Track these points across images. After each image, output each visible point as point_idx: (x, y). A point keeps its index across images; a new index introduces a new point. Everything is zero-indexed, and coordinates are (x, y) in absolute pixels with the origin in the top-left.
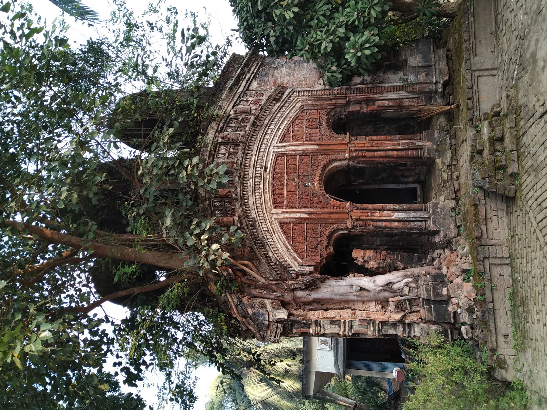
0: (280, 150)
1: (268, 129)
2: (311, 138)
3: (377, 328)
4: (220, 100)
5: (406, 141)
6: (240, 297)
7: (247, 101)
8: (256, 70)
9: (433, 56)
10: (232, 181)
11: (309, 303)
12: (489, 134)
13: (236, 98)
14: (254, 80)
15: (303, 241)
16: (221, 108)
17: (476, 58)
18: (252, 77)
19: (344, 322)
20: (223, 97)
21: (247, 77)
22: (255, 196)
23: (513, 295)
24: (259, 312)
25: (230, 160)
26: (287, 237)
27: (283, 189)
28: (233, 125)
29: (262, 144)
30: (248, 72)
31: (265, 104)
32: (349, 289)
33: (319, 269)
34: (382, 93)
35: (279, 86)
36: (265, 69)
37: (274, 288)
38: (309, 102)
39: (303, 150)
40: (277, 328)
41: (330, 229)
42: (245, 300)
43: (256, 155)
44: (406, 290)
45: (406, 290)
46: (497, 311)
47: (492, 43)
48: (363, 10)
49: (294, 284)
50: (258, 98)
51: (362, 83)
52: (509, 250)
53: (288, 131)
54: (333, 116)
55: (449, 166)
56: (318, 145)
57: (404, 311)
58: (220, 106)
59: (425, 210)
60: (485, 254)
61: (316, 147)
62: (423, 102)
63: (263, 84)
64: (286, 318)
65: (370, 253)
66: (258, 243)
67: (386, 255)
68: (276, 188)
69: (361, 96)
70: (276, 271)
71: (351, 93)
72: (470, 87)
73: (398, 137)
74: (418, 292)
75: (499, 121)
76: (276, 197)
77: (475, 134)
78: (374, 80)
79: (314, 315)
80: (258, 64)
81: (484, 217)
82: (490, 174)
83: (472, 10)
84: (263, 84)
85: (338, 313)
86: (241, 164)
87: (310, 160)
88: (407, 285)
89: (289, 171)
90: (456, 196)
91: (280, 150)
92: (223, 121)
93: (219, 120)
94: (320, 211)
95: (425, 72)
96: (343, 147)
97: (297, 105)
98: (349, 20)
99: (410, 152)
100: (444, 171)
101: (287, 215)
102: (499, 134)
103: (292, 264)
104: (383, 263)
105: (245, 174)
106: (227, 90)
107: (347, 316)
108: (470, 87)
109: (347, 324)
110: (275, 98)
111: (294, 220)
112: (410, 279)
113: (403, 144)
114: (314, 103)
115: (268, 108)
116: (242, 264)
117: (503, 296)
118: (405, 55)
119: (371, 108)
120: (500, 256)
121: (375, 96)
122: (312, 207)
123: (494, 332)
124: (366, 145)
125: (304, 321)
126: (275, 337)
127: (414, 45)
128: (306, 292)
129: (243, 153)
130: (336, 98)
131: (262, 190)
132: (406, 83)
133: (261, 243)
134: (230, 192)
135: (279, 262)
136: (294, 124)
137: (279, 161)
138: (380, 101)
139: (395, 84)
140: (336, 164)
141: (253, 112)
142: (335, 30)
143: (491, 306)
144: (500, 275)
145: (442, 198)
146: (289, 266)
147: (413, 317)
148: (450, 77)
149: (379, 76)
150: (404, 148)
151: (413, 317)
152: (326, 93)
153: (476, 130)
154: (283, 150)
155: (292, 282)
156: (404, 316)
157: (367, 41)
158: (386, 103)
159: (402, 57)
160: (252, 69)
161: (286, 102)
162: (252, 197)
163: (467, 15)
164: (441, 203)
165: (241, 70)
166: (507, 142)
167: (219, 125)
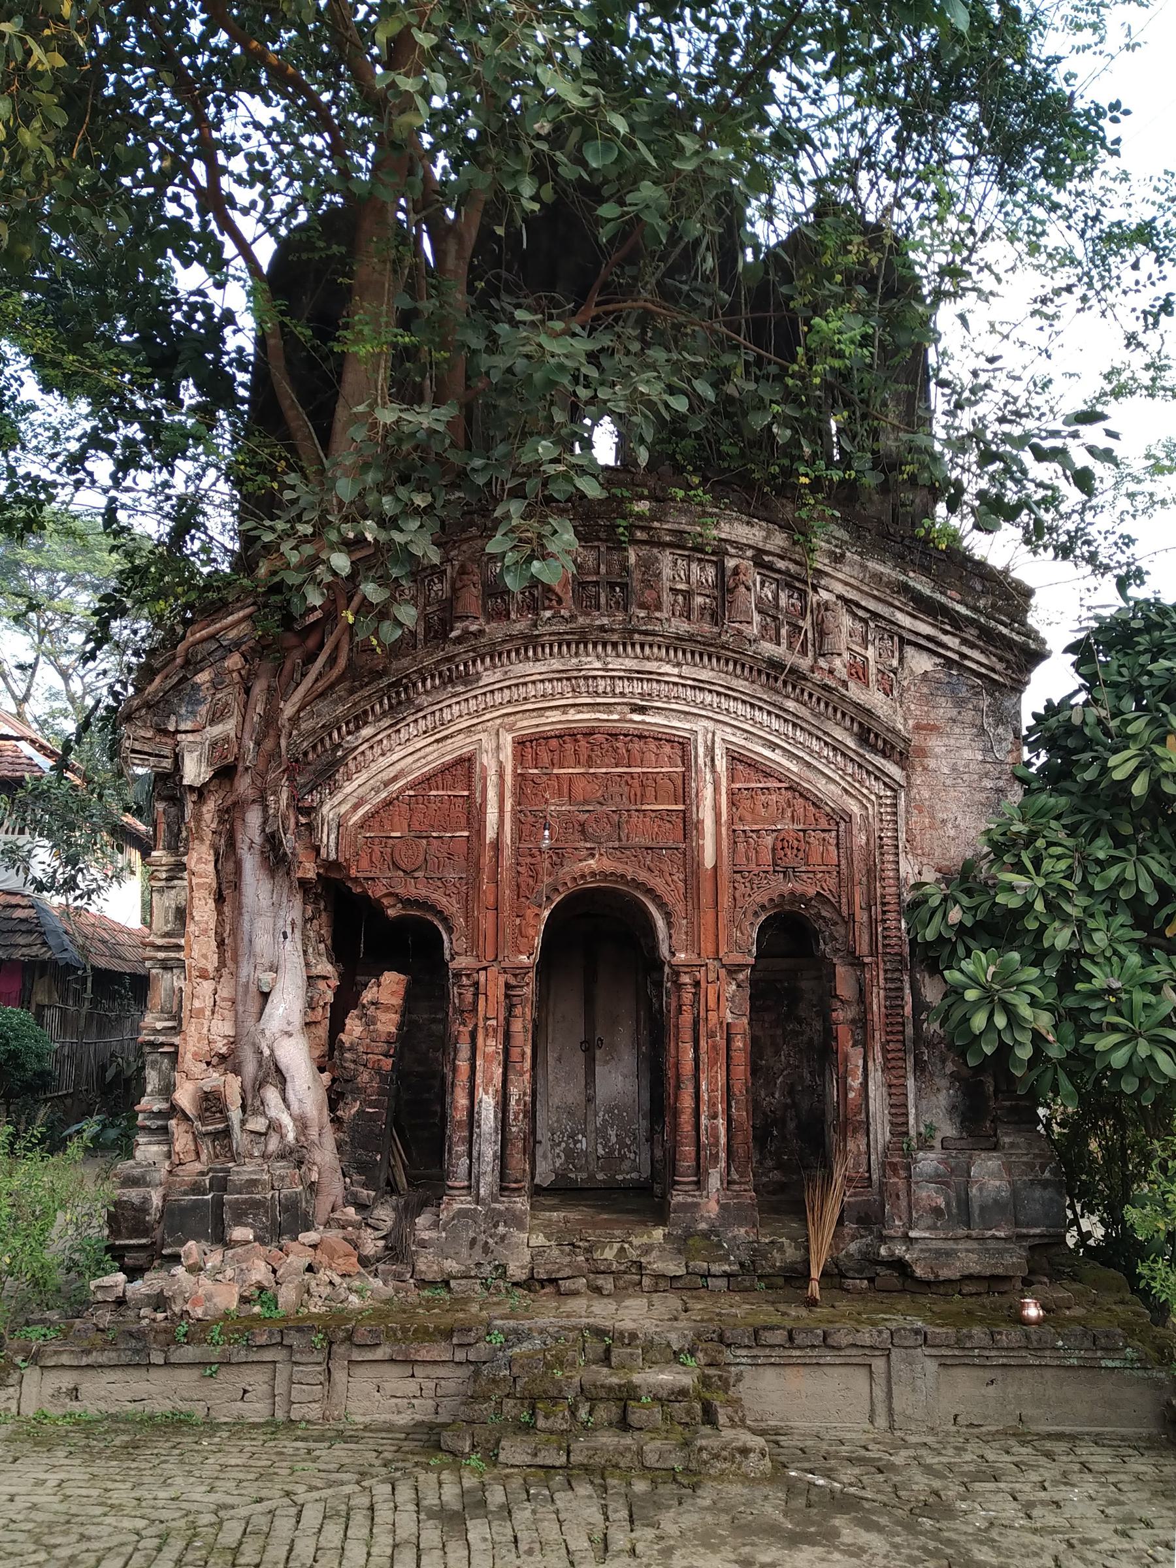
0: (701, 751)
1: (769, 713)
2: (741, 847)
3: (161, 1039)
4: (860, 554)
5: (723, 1140)
6: (244, 648)
7: (865, 643)
8: (974, 666)
9: (1002, 1234)
10: (598, 608)
11: (231, 843)
12: (649, 1385)
13: (872, 605)
14: (938, 661)
15: (416, 825)
16: (838, 559)
17: (931, 1366)
18: (949, 654)
19: (179, 948)
20: (872, 565)
21: (946, 639)
22: (550, 680)
23: (177, 1423)
24: (199, 702)
25: (667, 598)
26: (427, 781)
27: (578, 763)
29: (719, 694)
30: (964, 641)
31: (843, 698)
32: (265, 961)
36: (977, 694)
37: (268, 744)
39: (700, 822)
40: (157, 756)
41: (451, 906)
42: (234, 661)
46: (142, 1373)
47: (986, 1417)
48: (1125, 1009)
49: (277, 802)
50: (872, 678)
51: (920, 1005)
53: (767, 775)
54: (819, 916)
55: (640, 1266)
57: (200, 1118)
58: (843, 555)
59: (502, 1189)
60: (301, 1352)
61: (709, 861)
63: (925, 690)
64: (186, 782)
65: (388, 1023)
66: (398, 694)
67: (378, 1071)
68: (583, 743)
69: (877, 1002)
70: (314, 748)
71: (886, 971)
72: (830, 1341)
73: (740, 1114)
74: (251, 1156)
75: (687, 1420)
76: (554, 743)
77: (669, 1345)
78: (930, 1044)
80: (993, 670)
81: (413, 1357)
82: (520, 1383)
83: (1103, 1363)
84: (925, 690)
85: (206, 930)
86: (646, 633)
87: (670, 844)
88: (274, 1126)
89: (636, 783)
90: (543, 1283)
91: (701, 751)
92: (793, 568)
93: (797, 557)
94: (505, 875)
95: (948, 1204)
96: (708, 946)
97: (851, 801)
98: (1096, 964)
99: (688, 1149)
100: (622, 1249)
101: (492, 779)
102: (637, 1416)
104: (354, 1062)
105: (615, 645)
109: (173, 955)
110: (869, 730)
111: (479, 800)
112: (291, 1136)
113: (715, 1128)
114: (856, 854)
116: (336, 648)
117: (186, 1395)
118: (1012, 1145)
119: (844, 1034)
121: (878, 1048)
122: (517, 852)
125: (184, 834)
126: (134, 751)
127: (1047, 1174)
128: (258, 839)
129: (679, 638)
131: (570, 701)
132: (914, 1143)
133: (400, 703)
134: (560, 601)
135: (344, 757)
136: (789, 794)
137: (667, 749)
138: (861, 1062)
139: (912, 1111)
140: (660, 923)
141: (822, 663)
142: (1066, 919)
143: (157, 1358)
144: (245, 1391)
145: (539, 1240)
146: (335, 788)
147: (182, 1141)
148: (928, 1283)
149: (943, 1062)
151: (182, 1141)
152: (888, 890)
153: (681, 1350)
155: (284, 796)
156: (186, 1118)
157: (1014, 1019)
158: (855, 1083)
159: (1007, 1134)
161: (860, 766)
162: (544, 669)
163: (1087, 1343)
165: (967, 618)
166: (608, 1440)
167: (782, 558)
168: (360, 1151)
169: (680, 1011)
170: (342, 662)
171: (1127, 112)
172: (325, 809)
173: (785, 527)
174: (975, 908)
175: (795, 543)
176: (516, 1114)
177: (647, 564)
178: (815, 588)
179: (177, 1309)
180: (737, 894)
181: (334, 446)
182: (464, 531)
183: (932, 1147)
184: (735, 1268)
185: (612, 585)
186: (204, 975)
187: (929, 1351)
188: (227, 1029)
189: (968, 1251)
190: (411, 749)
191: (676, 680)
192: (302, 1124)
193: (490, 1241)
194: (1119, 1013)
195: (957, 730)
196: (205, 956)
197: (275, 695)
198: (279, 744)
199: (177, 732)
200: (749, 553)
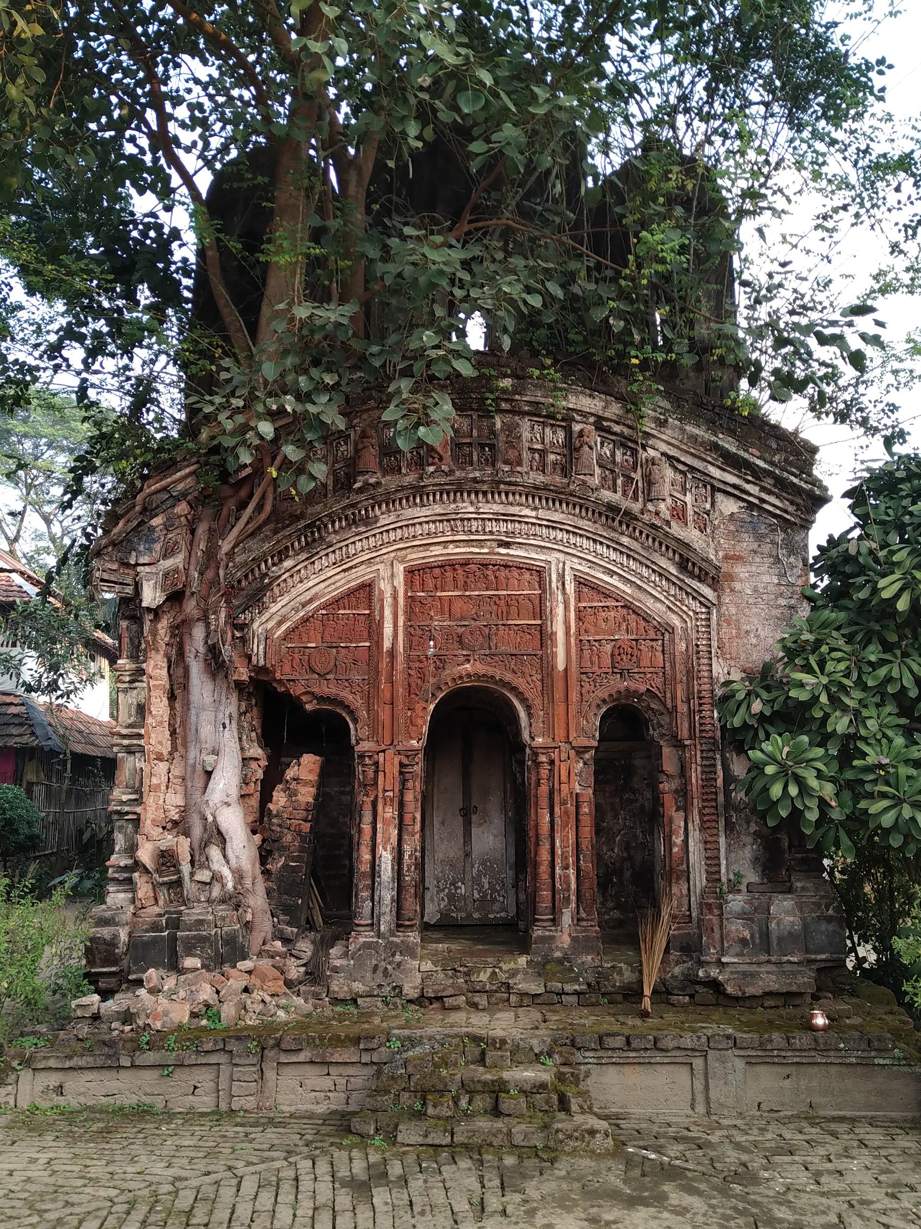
0: (554, 577)
1: (608, 547)
2: (587, 653)
3: (127, 809)
4: (680, 420)
5: (573, 886)
6: (189, 497)
7: (684, 490)
8: (771, 508)
9: (795, 959)
12: (516, 1081)
13: (689, 460)
15: (327, 638)
16: (662, 424)
17: (740, 1064)
18: (751, 499)
19: (140, 736)
20: (689, 428)
21: (748, 487)
23: (141, 1113)
24: (154, 541)
25: (526, 455)
26: (336, 602)
27: (456, 587)
28: (619, 458)
29: (568, 532)
30: (763, 489)
31: (666, 534)
32: (209, 746)
33: (263, 678)
34: (702, 829)
35: (718, 568)
36: (773, 531)
37: (210, 574)
38: (683, 646)
39: (554, 634)
40: (121, 584)
41: (356, 701)
42: (182, 508)
43: (537, 518)
44: (204, 875)
45: (204, 875)
46: (113, 1073)
48: (892, 781)
49: (217, 620)
50: (690, 518)
51: (729, 778)
52: (246, 1111)
53: (607, 596)
54: (649, 708)
55: (508, 987)
56: (566, 670)
57: (157, 871)
58: (666, 421)
59: (399, 926)
60: (240, 1056)
61: (561, 665)
62: (678, 929)
63: (732, 528)
64: (144, 604)
65: (306, 795)
66: (313, 533)
67: (299, 833)
68: (460, 571)
69: (695, 776)
71: (702, 751)
72: (659, 1045)
73: (587, 865)
74: (199, 901)
75: (546, 1108)
77: (531, 1049)
78: (737, 809)
79: (156, 666)
80: (786, 511)
81: (328, 1060)
82: (414, 1079)
83: (876, 1061)
84: (732, 528)
85: (161, 722)
86: (509, 484)
87: (530, 651)
88: (217, 878)
90: (431, 1000)
91: (554, 577)
92: (626, 431)
93: (629, 422)
94: (399, 677)
95: (752, 936)
96: (560, 733)
97: (674, 616)
98: (869, 744)
99: (546, 893)
100: (494, 973)
101: (388, 601)
102: (506, 1105)
103: (267, 615)
104: (280, 826)
105: (485, 493)
106: (709, 436)
107: (153, 741)
108: (659, 1045)
109: (135, 742)
110: (688, 560)
111: (378, 618)
112: (230, 885)
113: (567, 877)
115: (661, 544)
116: (263, 497)
117: (148, 1090)
119: (669, 801)
120: (234, 1089)
121: (696, 812)
122: (408, 659)
123: (68, 1064)
124: (564, 787)
125: (143, 646)
126: (102, 580)
127: (831, 912)
128: (202, 650)
129: (536, 488)
130: (691, 713)
131: (450, 538)
132: (725, 888)
133: (314, 540)
135: (270, 584)
136: (625, 611)
137: (527, 576)
138: (682, 824)
139: (724, 862)
140: (522, 714)
141: (650, 507)
142: (845, 709)
143: (125, 1061)
144: (195, 1088)
145: (428, 966)
146: (263, 609)
149: (748, 823)
150: (557, 879)
151: (144, 890)
152: (704, 687)
153: (541, 1053)
154: (554, 585)
155: (223, 615)
156: (147, 871)
158: (678, 840)
159: (799, 880)
160: (772, 499)
161: (681, 589)
163: (864, 1046)
164: (416, 963)
165: (765, 470)
166: (484, 1124)
167: (618, 423)
168: (285, 897)
169: (538, 784)
170: (268, 508)
171: (890, 67)
172: (255, 626)
173: (620, 398)
174: (773, 701)
175: (628, 411)
176: (409, 866)
177: (511, 429)
178: (644, 447)
179: (141, 1023)
180: (584, 691)
181: (260, 336)
182: (364, 403)
183: (739, 891)
184: (584, 987)
185: (482, 446)
186: (160, 758)
187: (737, 1052)
188: (179, 800)
189: (768, 973)
190: (323, 577)
191: (534, 521)
192: (239, 876)
193: (389, 967)
194: (888, 784)
195: (758, 560)
196: (160, 743)
197: (214, 535)
198: (218, 575)
199: (137, 564)
200: (592, 419)
